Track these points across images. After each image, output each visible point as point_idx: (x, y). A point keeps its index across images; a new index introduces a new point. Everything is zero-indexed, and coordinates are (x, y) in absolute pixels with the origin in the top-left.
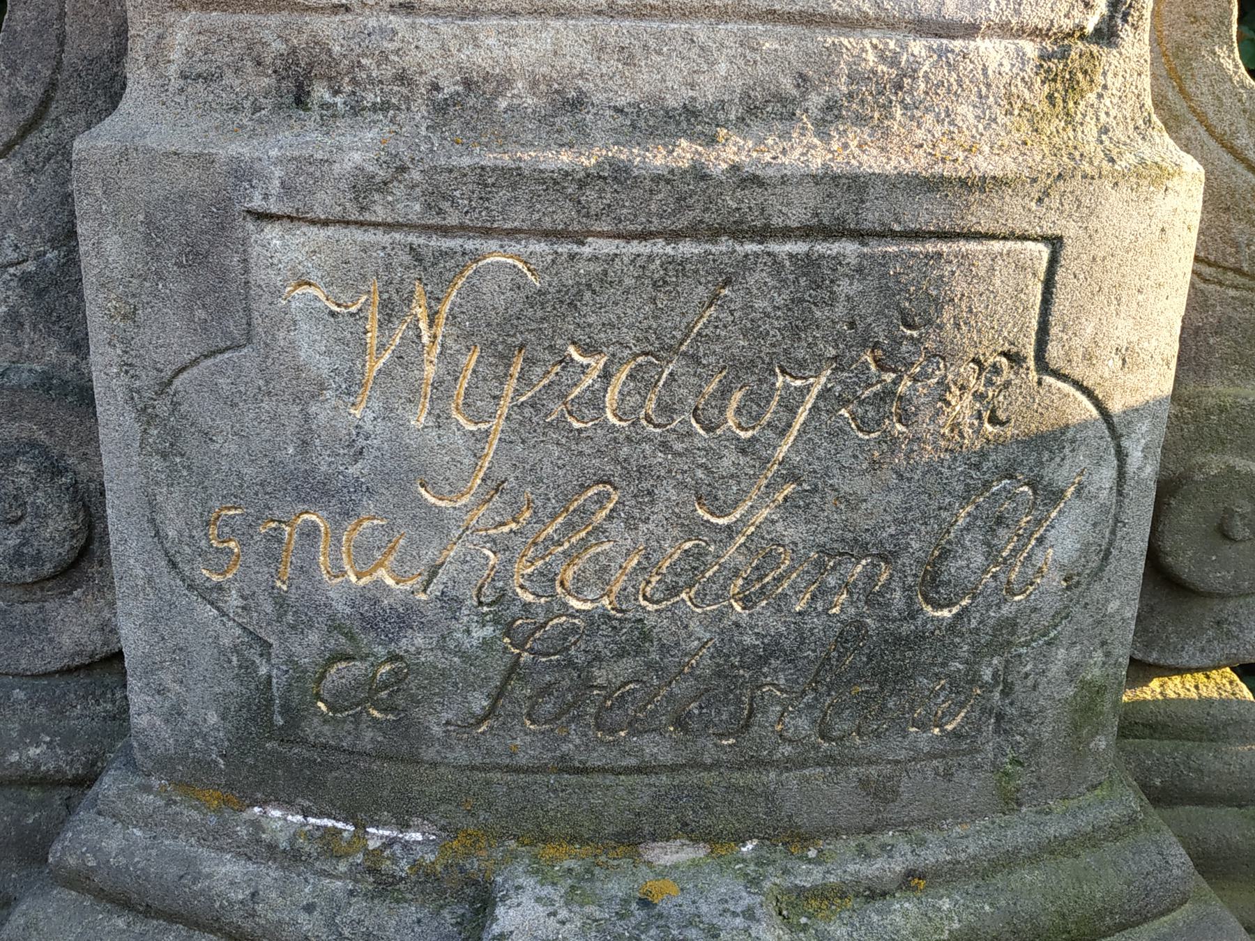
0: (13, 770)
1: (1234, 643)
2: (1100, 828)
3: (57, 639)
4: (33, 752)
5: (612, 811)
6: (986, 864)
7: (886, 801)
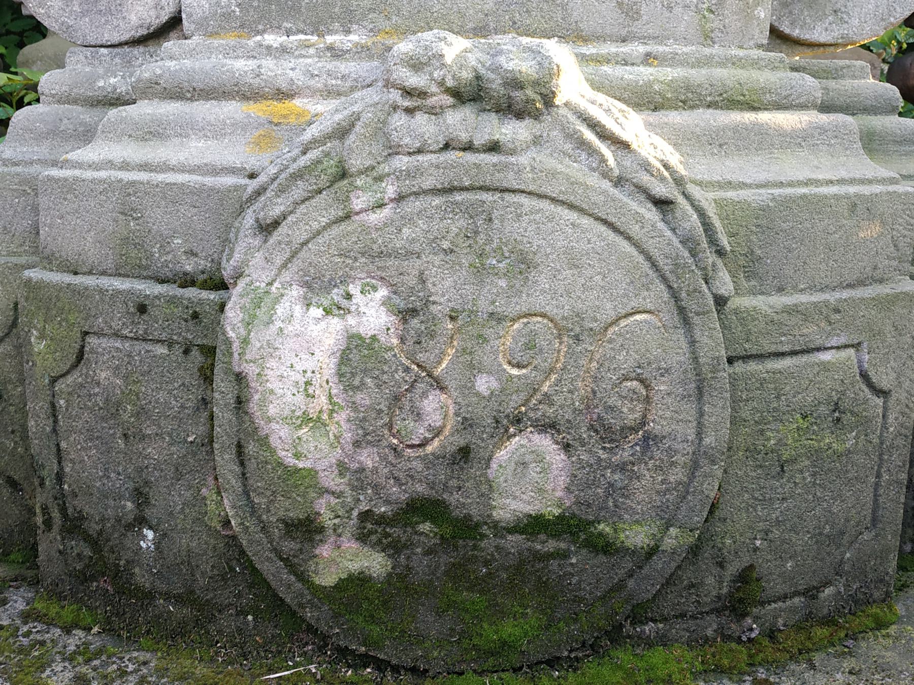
0: (100, 91)
1: (845, 26)
2: (762, 59)
3: (128, 17)
4: (112, 80)
5: (471, 12)
6: (693, 60)
7: (635, 20)
